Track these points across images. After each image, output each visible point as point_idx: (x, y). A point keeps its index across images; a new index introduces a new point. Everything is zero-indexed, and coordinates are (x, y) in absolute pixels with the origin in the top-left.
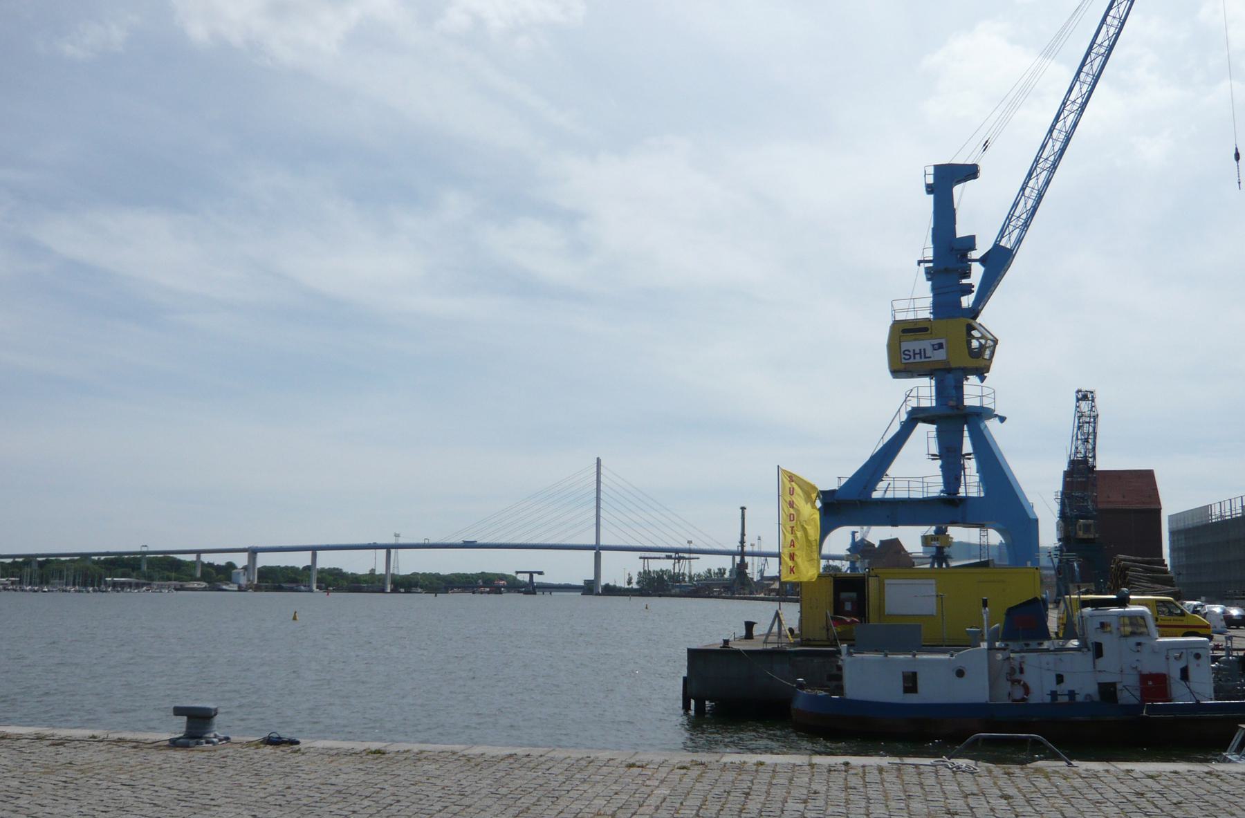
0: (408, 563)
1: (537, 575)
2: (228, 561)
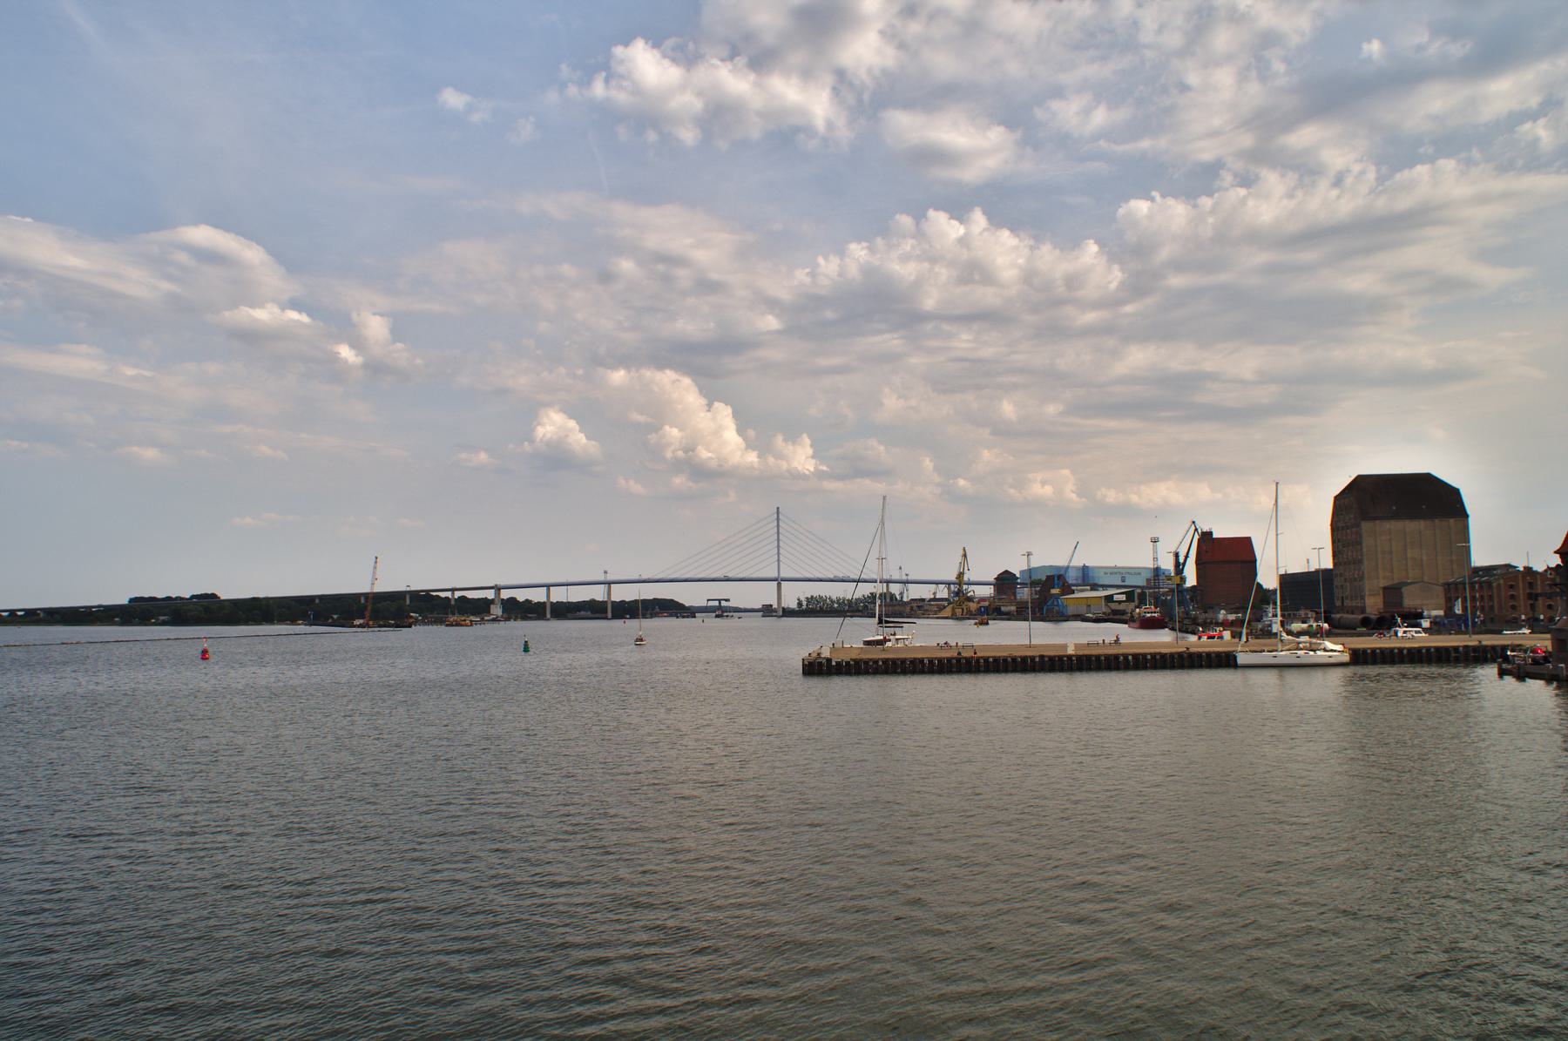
0: (621, 594)
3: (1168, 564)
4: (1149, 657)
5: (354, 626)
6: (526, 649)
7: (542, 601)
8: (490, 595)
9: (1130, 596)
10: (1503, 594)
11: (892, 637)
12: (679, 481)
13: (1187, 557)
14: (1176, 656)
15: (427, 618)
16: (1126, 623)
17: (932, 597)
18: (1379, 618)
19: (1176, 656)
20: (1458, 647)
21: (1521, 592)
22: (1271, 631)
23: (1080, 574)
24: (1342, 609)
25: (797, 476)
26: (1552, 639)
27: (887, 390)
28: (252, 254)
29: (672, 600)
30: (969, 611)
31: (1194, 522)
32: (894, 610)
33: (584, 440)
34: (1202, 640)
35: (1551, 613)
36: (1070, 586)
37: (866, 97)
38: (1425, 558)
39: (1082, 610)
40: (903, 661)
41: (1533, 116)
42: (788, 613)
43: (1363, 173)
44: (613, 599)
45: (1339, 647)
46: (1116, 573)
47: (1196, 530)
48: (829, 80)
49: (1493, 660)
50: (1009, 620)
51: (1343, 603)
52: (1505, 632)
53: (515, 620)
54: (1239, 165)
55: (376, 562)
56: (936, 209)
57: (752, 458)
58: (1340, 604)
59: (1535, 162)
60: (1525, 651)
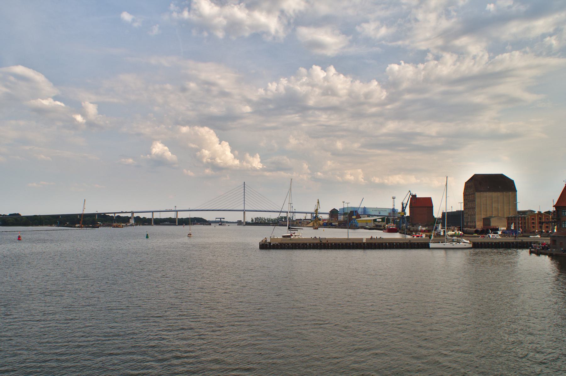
0: (182, 215)
3: (399, 209)
4: (395, 244)
5: (76, 227)
6: (147, 237)
8: (129, 215)
9: (383, 220)
10: (530, 221)
11: (293, 234)
12: (208, 171)
13: (407, 205)
14: (405, 244)
15: (104, 224)
16: (382, 230)
17: (305, 218)
18: (482, 230)
19: (405, 244)
20: (514, 242)
21: (537, 221)
22: (440, 234)
23: (363, 211)
24: (467, 226)
25: (254, 170)
26: (550, 240)
27: (291, 136)
28: (39, 78)
29: (202, 218)
30: (320, 225)
31: (410, 191)
32: (294, 224)
33: (171, 155)
34: (414, 237)
35: (547, 229)
36: (359, 215)
37: (292, 21)
38: (499, 207)
39: (364, 225)
40: (299, 244)
41: (551, 35)
42: (247, 224)
43: (483, 56)
44: (178, 218)
45: (468, 242)
46: (377, 210)
47: (411, 194)
48: (278, 14)
49: (527, 248)
50: (335, 228)
51: (467, 224)
52: (531, 237)
53: (139, 225)
54: (435, 51)
55: (85, 202)
56: (316, 65)
57: (237, 162)
58: (466, 224)
59: (550, 52)
60: (539, 244)
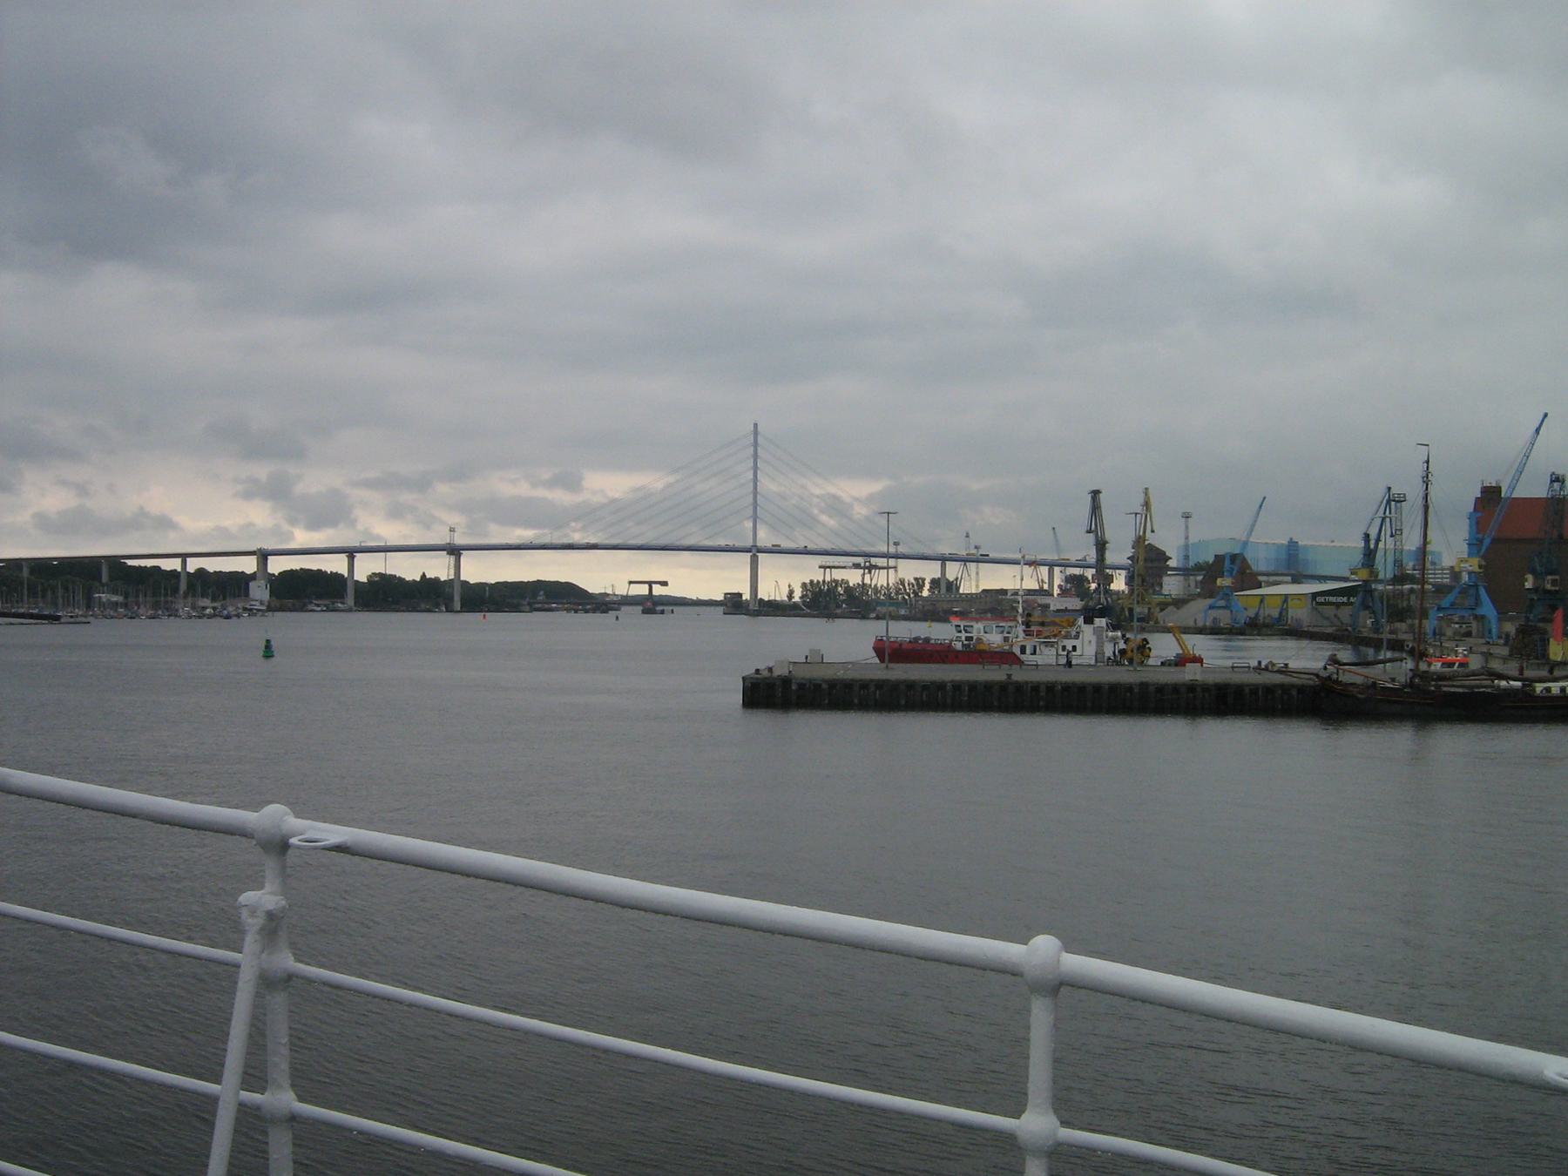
1: (658, 585)
2: (202, 566)
7: (936, 577)
8: (248, 565)
36: (1255, 575)
